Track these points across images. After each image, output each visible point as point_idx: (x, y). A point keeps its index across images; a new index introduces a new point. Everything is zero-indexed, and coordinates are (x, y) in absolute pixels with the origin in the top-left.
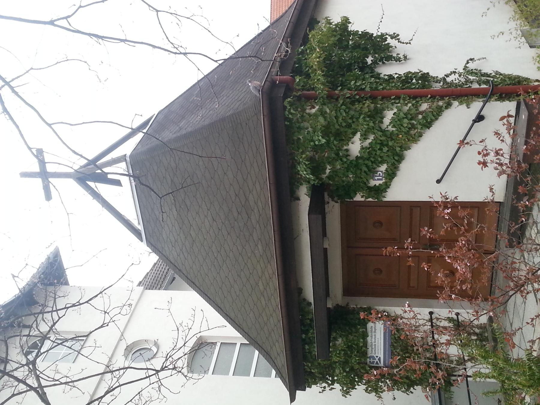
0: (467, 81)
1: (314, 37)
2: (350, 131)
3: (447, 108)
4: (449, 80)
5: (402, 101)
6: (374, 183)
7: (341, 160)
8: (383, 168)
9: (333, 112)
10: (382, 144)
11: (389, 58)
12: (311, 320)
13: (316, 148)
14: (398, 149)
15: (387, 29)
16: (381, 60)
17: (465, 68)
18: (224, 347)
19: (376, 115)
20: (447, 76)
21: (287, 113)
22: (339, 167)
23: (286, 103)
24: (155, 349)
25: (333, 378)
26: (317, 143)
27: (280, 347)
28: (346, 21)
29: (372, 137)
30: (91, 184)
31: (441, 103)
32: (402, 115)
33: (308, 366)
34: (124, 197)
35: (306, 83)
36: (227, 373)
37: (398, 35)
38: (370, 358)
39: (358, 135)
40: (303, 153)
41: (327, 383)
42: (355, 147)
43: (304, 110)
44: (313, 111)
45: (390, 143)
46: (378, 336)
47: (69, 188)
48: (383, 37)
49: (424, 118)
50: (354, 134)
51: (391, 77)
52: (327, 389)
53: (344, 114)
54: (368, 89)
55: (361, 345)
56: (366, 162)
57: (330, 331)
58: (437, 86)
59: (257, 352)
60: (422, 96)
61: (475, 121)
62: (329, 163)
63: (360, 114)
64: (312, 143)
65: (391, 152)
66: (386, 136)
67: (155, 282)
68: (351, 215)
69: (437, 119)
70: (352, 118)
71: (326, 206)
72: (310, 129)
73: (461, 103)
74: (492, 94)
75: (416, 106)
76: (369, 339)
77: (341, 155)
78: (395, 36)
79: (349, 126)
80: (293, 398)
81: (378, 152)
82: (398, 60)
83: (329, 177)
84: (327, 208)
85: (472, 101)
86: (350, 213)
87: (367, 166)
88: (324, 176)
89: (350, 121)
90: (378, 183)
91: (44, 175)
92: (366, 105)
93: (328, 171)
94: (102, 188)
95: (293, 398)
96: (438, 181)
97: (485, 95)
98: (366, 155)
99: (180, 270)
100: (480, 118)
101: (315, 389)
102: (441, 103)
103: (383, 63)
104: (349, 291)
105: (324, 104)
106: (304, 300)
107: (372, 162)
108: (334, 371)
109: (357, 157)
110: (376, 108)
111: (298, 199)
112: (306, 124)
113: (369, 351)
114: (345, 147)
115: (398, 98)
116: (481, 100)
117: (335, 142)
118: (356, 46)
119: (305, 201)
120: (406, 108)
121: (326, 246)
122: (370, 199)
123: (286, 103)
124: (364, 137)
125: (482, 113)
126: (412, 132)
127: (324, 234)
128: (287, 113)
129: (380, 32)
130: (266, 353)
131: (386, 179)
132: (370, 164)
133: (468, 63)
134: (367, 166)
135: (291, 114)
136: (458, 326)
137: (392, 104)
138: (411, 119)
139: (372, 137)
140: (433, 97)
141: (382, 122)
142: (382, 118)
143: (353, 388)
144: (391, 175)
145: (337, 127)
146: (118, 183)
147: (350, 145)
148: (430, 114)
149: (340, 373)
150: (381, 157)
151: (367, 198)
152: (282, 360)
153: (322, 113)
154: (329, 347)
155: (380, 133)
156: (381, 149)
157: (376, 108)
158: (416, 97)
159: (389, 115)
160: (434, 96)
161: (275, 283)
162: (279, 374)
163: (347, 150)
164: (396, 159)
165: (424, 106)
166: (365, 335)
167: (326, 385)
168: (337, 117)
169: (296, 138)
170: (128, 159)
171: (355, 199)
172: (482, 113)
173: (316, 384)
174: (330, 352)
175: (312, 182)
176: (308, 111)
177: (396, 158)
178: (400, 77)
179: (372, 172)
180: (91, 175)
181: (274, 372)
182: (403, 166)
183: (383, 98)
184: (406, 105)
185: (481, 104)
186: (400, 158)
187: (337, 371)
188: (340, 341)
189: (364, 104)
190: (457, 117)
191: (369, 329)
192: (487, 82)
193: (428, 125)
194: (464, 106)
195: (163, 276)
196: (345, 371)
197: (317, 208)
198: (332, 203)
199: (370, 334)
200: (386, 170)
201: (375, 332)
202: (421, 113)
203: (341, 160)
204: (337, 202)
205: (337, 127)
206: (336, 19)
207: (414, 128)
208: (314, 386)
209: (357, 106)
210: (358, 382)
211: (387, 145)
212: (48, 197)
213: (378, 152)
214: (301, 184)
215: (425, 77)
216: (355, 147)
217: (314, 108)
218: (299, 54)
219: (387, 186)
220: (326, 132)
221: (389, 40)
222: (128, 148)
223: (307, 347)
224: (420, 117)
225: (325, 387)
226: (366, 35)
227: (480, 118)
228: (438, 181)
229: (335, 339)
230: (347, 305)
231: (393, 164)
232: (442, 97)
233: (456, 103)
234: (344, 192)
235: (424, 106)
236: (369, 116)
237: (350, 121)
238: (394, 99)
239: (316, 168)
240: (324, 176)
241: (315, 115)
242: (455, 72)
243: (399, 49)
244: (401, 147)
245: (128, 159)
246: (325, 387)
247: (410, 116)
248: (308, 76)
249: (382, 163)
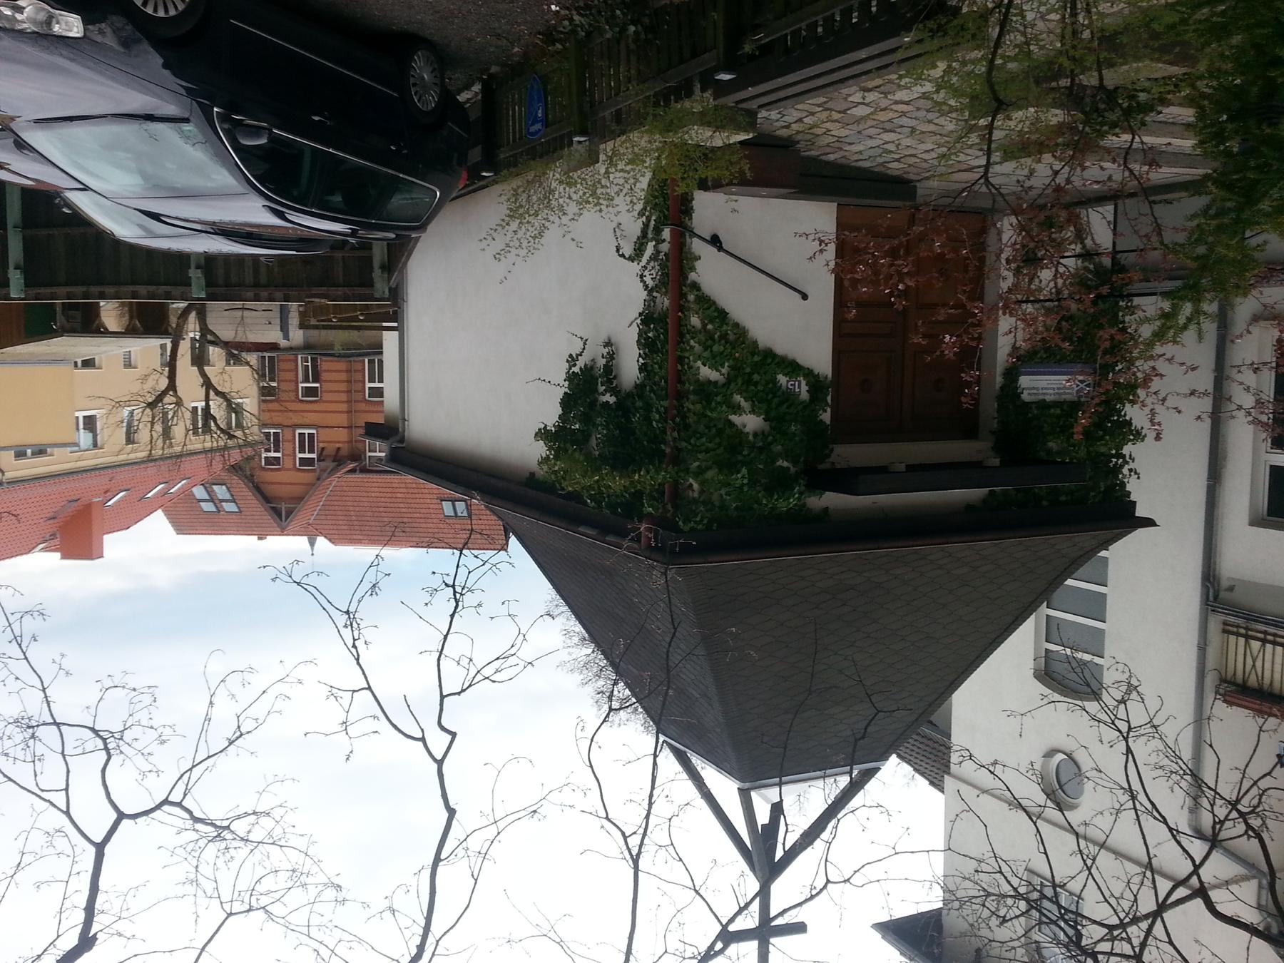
0: (654, 258)
1: (578, 481)
2: (728, 431)
3: (699, 289)
4: (650, 283)
5: (687, 354)
6: (805, 395)
7: (770, 444)
8: (782, 379)
9: (700, 456)
10: (749, 382)
11: (608, 369)
12: (1018, 491)
13: (753, 482)
14: (756, 358)
15: (559, 374)
16: (610, 381)
17: (631, 259)
18: (1055, 636)
19: (706, 391)
20: (646, 287)
21: (700, 527)
22: (779, 447)
23: (686, 528)
24: (1060, 756)
25: (1113, 456)
26: (746, 481)
27: (1062, 543)
28: (543, 434)
29: (738, 398)
30: (779, 853)
31: (691, 297)
32: (706, 354)
33: (1094, 497)
34: (804, 800)
35: (652, 498)
36: (1101, 632)
37: (571, 356)
38: (1080, 397)
39: (733, 418)
40: (760, 504)
41: (1122, 466)
42: (750, 422)
43: (695, 501)
44: (696, 486)
45: (748, 370)
46: (1044, 384)
47: (785, 890)
48: (571, 377)
49: (711, 322)
50: (731, 424)
51: (642, 368)
52: (1132, 465)
53: (704, 440)
54: (665, 403)
55: (1058, 411)
56: (774, 405)
57: (611, 356)
58: (664, 302)
59: (1069, 582)
60: (681, 324)
61: (720, 248)
62: (773, 462)
63: (706, 416)
64: (746, 489)
65: (758, 367)
66: (736, 376)
67: (934, 762)
68: (852, 427)
69: (714, 303)
70: (708, 427)
71: (838, 466)
72: (723, 492)
73: (693, 269)
74: (681, 224)
75: (694, 333)
76: (1048, 398)
77: (763, 443)
78: (572, 360)
79: (720, 432)
80: (1149, 523)
81: (760, 388)
82: (611, 356)
83: (795, 463)
84: (841, 464)
85: (691, 253)
86: (848, 429)
87: (781, 403)
88: (793, 470)
89: (714, 430)
90: (804, 388)
91: (765, 931)
92: (691, 407)
93: (786, 464)
94: (788, 837)
95: (1149, 523)
96: (805, 297)
97: (682, 235)
98: (764, 406)
99: (930, 705)
100: (715, 241)
101: (1132, 486)
102: (691, 297)
103: (615, 378)
104: (967, 427)
105: (687, 471)
106: (984, 501)
107: (775, 396)
108: (1103, 454)
109: (765, 420)
110: (695, 392)
111: (826, 509)
112: (715, 497)
113: (1068, 397)
114: (751, 437)
115: (681, 360)
116: (688, 239)
117: (745, 453)
118: (586, 419)
119: (832, 500)
120: (698, 348)
121: (902, 467)
122: (829, 399)
123: (686, 528)
124: (737, 409)
125: (708, 238)
126: (731, 337)
127: (883, 470)
128: (700, 527)
129: (562, 383)
130: (1070, 570)
131: (798, 375)
132: (776, 400)
133: (623, 256)
134: (781, 403)
135: (702, 520)
136: (1029, 260)
137: (690, 368)
138: (713, 340)
139: (738, 398)
140: (681, 309)
141: (716, 382)
142: (710, 382)
143: (1129, 423)
144: (793, 367)
145: (721, 450)
146: (777, 810)
147: (747, 430)
148: (708, 312)
149: (1106, 445)
150: (767, 383)
151: (827, 404)
152: (1084, 539)
153: (699, 473)
154: (1063, 462)
155: (733, 385)
156: (756, 384)
157: (695, 392)
158: (682, 331)
159: (706, 372)
160: (680, 305)
161: (959, 548)
162: (1105, 545)
163: (755, 434)
164: (771, 361)
165: (695, 321)
166: (1043, 405)
167: (1127, 467)
168: (707, 451)
169: (735, 514)
170: (747, 785)
171: (828, 422)
172: (708, 238)
173: (1123, 485)
174: (1071, 463)
175: (803, 488)
176: (696, 495)
177: (769, 361)
178: (645, 357)
179: (789, 397)
180: (765, 855)
181: (1103, 553)
182: (781, 348)
183: (680, 381)
184: (692, 348)
185: (695, 240)
186: (769, 354)
187: (1103, 449)
188: (1053, 445)
189: (689, 410)
190: (713, 274)
191: (1032, 398)
192: (658, 231)
193: (722, 315)
194: (698, 264)
195: (924, 740)
196: (1102, 438)
197: (846, 480)
198: (834, 458)
199: (1041, 397)
200: (786, 375)
201: (1037, 389)
202: (704, 325)
203: (770, 444)
204: (832, 450)
205: (721, 450)
206: (540, 449)
207: (726, 335)
208: (1128, 488)
209: (691, 419)
210: (1119, 416)
211: (750, 374)
212: (800, 928)
213: (760, 388)
214: (804, 505)
215: (648, 318)
216: (750, 422)
217: (691, 485)
218: (600, 507)
219: (809, 374)
220: (728, 466)
221: (576, 369)
222: (725, 787)
223: (1063, 498)
224: (710, 327)
225: (1130, 470)
226: (566, 402)
227: (715, 241)
228: (805, 297)
229: (1049, 452)
230: (993, 433)
231: (778, 364)
232: (683, 296)
233: (692, 276)
234: (820, 439)
235: (695, 321)
236: (709, 403)
237: (714, 430)
238: (682, 365)
239: (780, 483)
240: (793, 470)
241: (702, 484)
242: (642, 276)
243: (596, 353)
244: (753, 354)
245: (747, 785)
246: (1130, 470)
247: (710, 342)
248: (638, 495)
249: (774, 381)
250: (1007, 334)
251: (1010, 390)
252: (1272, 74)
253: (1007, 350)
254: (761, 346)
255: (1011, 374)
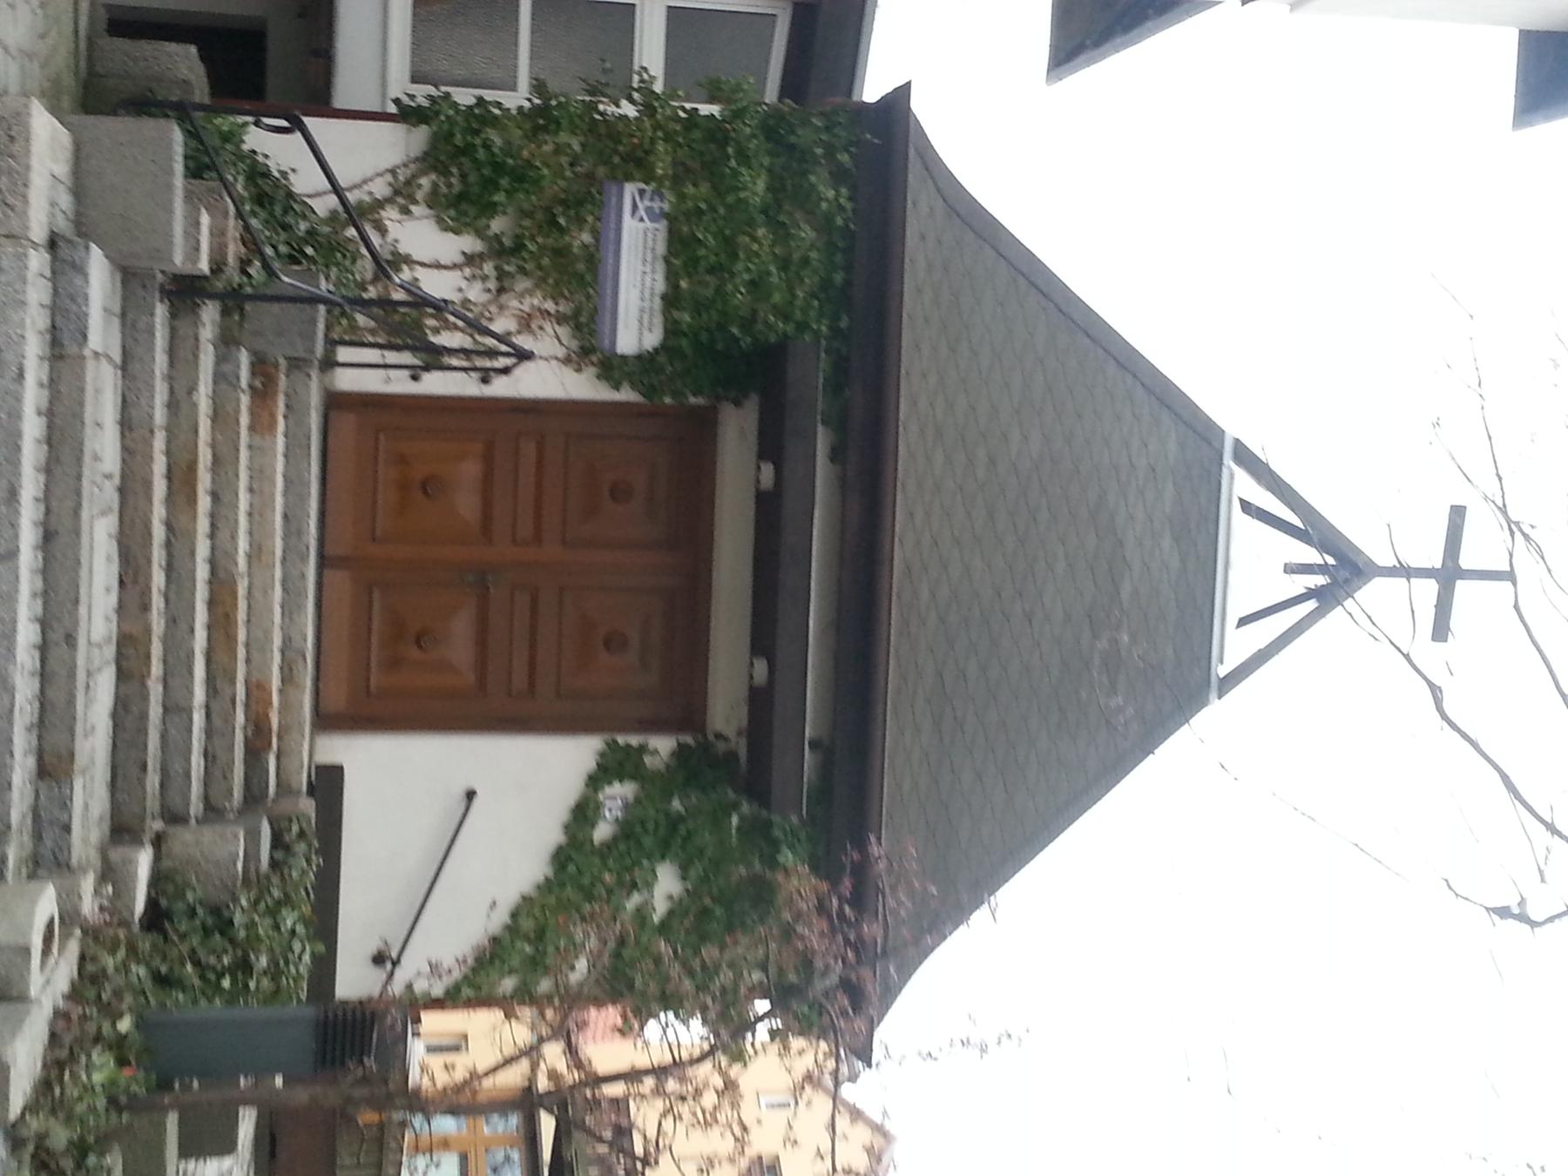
8: (602, 832)
71: (745, 723)
144: (583, 813)
182: (554, 836)
186: (561, 858)
198: (730, 731)
201: (642, 310)
216: (666, 884)
219: (596, 780)
234: (696, 765)
250: (547, 377)
251: (640, 369)
252: (661, 147)
253: (568, 374)
254: (534, 894)
255: (612, 368)
